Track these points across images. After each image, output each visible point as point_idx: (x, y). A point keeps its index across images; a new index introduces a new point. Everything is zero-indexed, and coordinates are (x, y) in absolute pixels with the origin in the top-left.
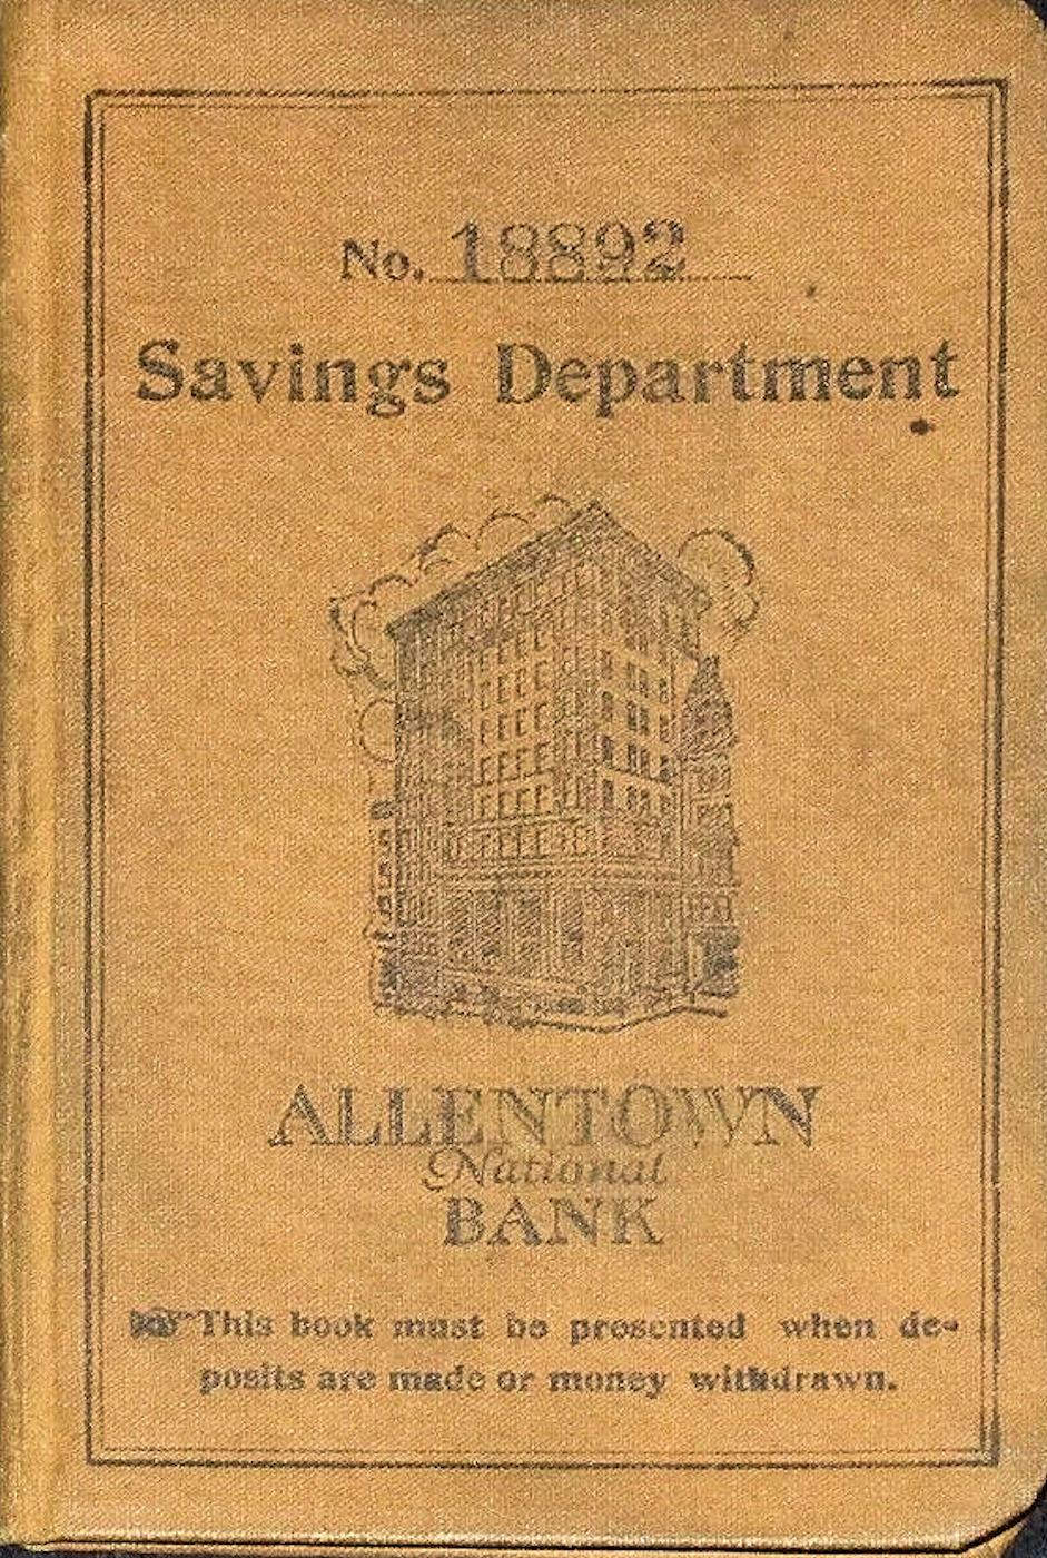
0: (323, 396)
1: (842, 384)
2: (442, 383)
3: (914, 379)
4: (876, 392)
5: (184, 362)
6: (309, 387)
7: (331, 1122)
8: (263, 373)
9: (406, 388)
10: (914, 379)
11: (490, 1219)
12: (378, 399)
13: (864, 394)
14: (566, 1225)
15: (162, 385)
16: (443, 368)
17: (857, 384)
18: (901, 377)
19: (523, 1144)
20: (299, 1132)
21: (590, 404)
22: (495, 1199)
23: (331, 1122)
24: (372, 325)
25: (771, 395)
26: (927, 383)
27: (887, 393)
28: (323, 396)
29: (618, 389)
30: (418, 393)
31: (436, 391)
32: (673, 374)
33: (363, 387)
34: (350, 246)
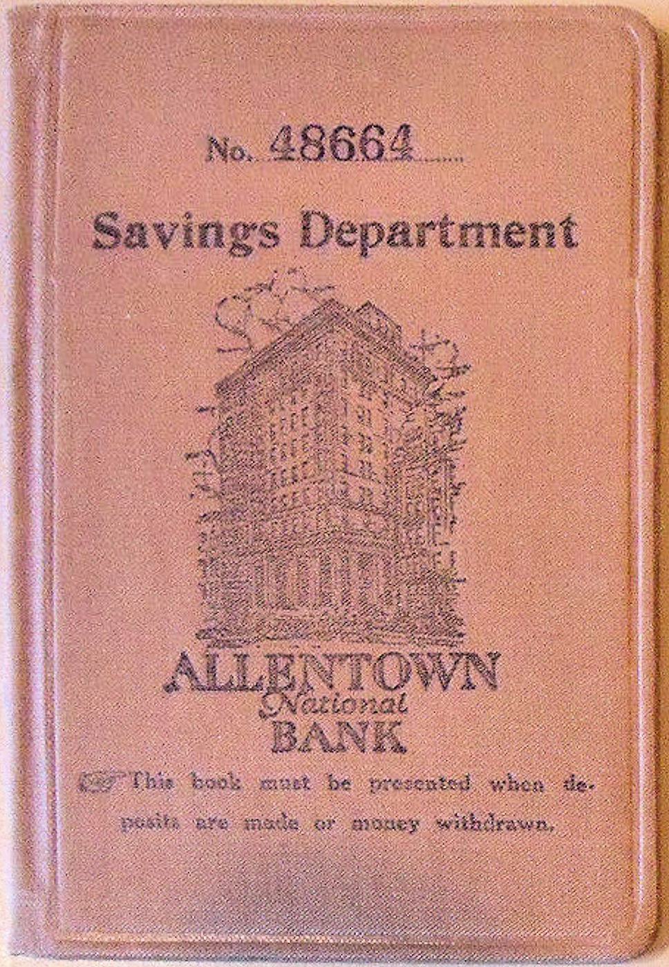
0: (203, 243)
1: (339, 239)
2: (275, 237)
3: (551, 236)
4: (528, 243)
5: (121, 226)
6: (195, 238)
7: (201, 674)
8: (167, 230)
9: (254, 239)
10: (551, 236)
11: (300, 735)
12: (234, 246)
13: (520, 244)
14: (347, 741)
15: (107, 240)
16: (276, 226)
17: (347, 237)
18: (542, 235)
19: (320, 690)
20: (182, 680)
21: (357, 248)
22: (302, 722)
23: (201, 674)
24: (224, 196)
25: (480, 244)
26: (559, 239)
27: (535, 244)
28: (203, 243)
29: (372, 239)
30: (261, 243)
31: (272, 242)
32: (405, 232)
33: (227, 239)
34: (212, 141)
